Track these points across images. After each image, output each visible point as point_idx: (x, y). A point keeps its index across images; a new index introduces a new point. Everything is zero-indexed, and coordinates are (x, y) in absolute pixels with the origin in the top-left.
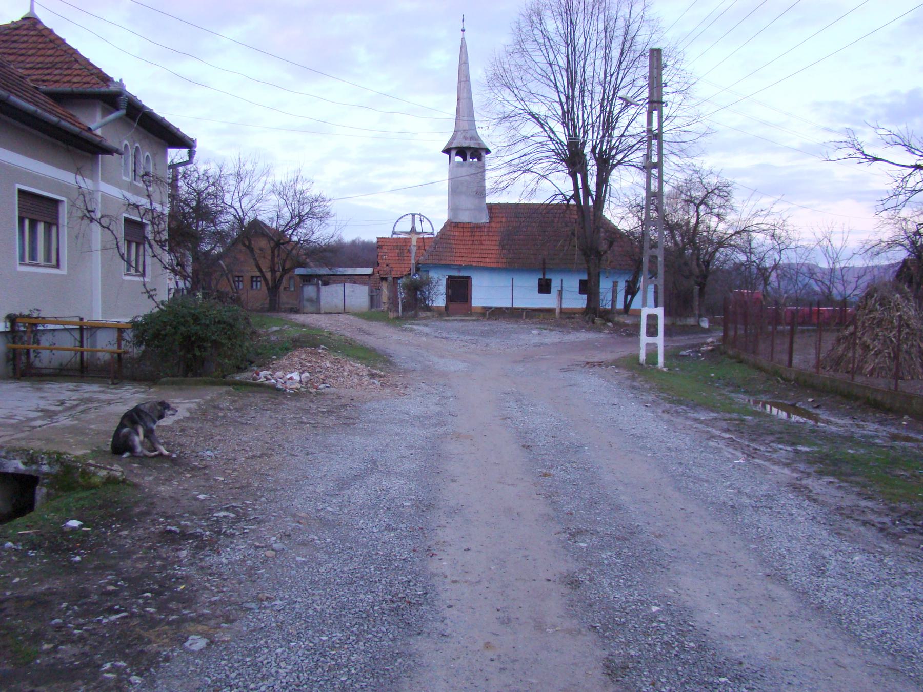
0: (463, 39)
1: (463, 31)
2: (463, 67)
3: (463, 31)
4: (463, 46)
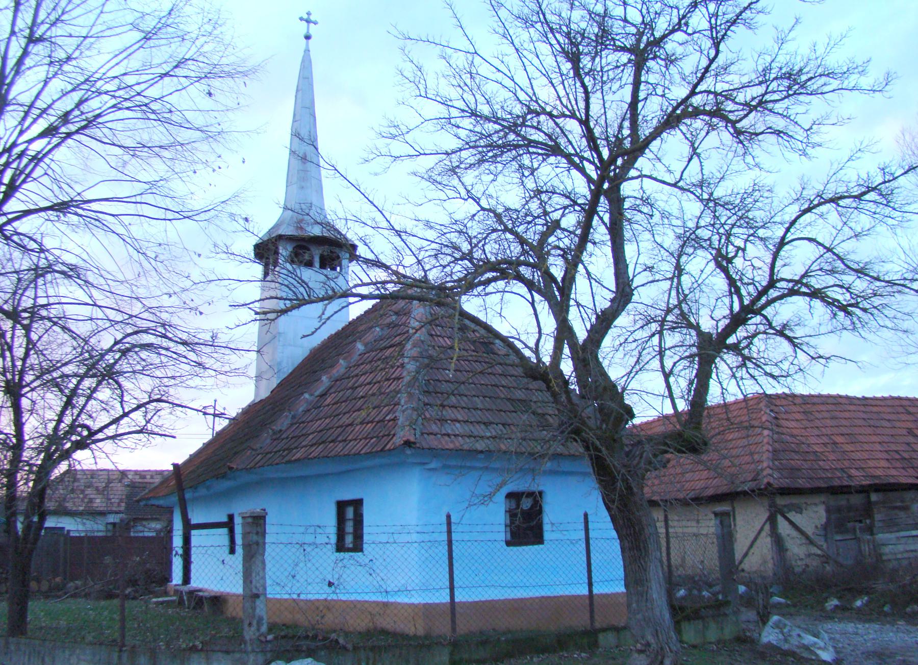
0: (307, 51)
1: (308, 37)
3: (308, 37)
4: (306, 64)
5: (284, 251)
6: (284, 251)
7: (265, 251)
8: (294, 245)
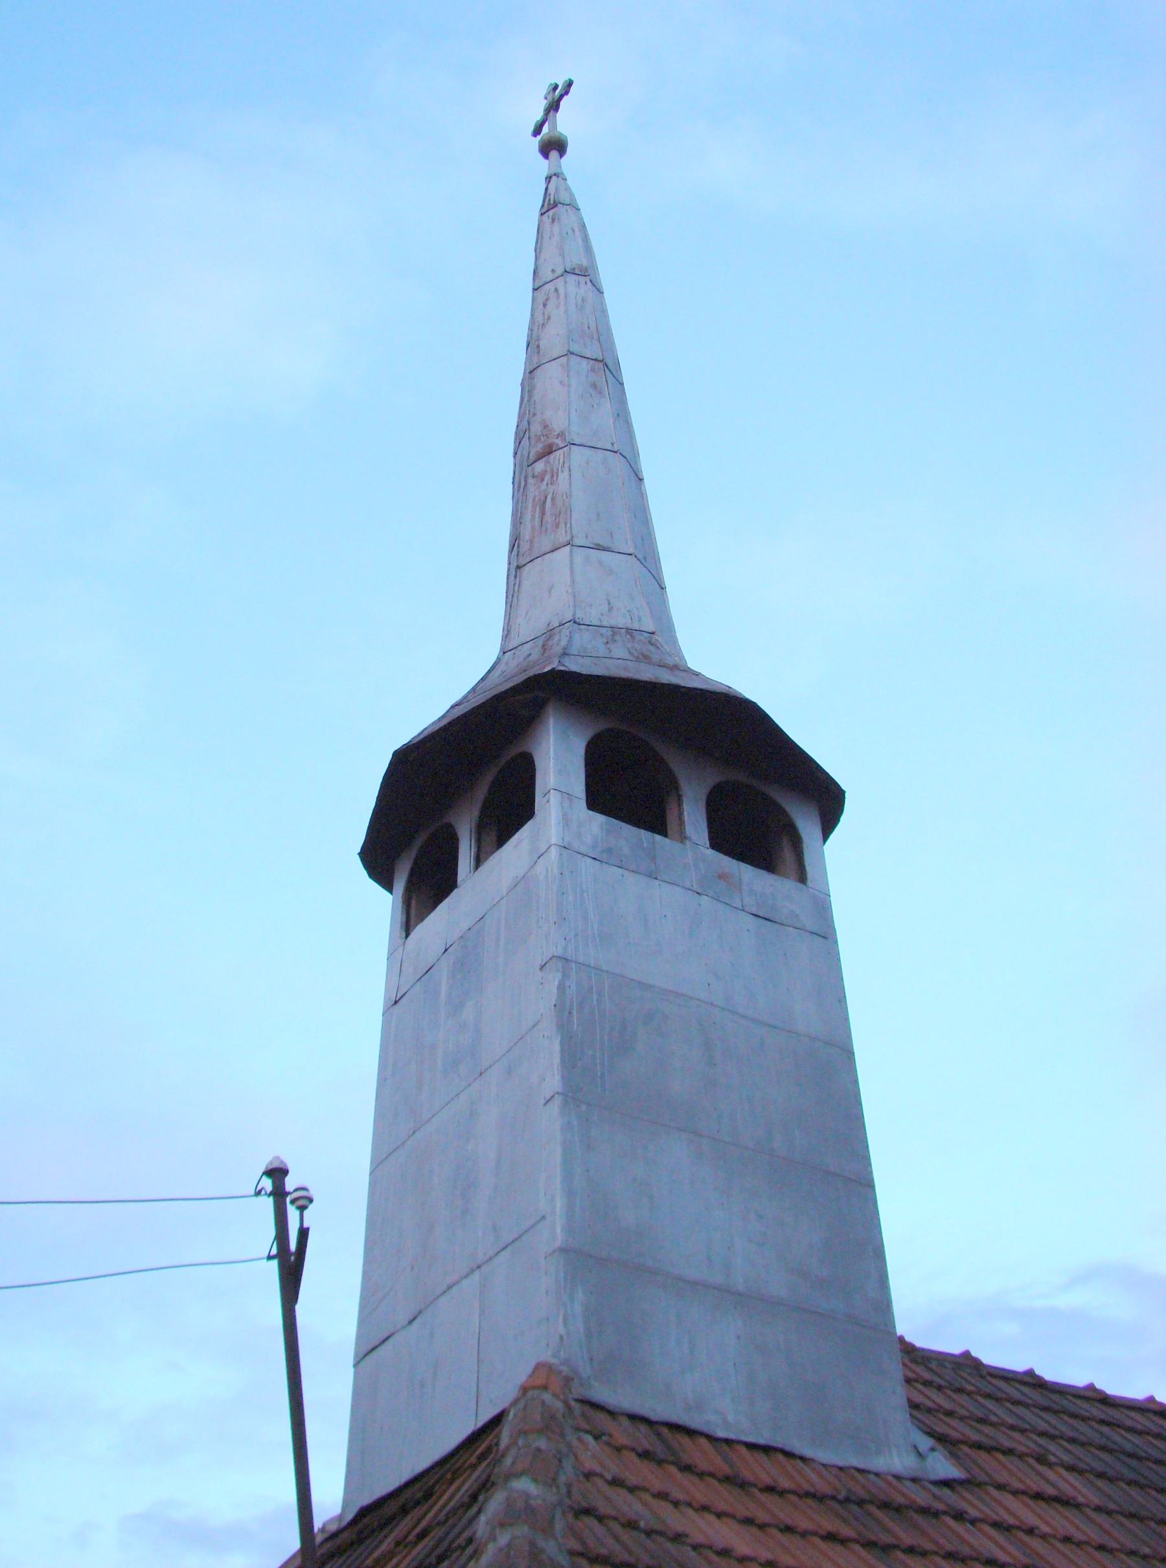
1: (554, 147)
2: (572, 288)
5: (559, 758)
6: (559, 758)
7: (437, 809)
8: (602, 725)
